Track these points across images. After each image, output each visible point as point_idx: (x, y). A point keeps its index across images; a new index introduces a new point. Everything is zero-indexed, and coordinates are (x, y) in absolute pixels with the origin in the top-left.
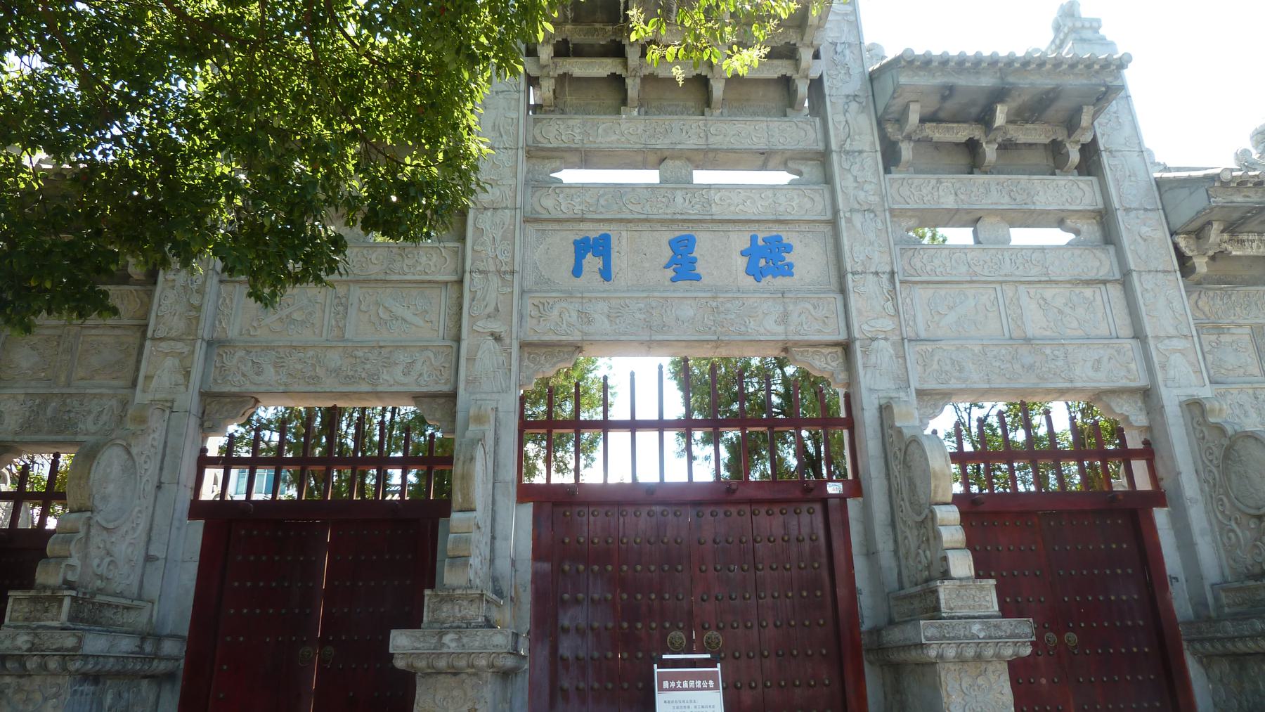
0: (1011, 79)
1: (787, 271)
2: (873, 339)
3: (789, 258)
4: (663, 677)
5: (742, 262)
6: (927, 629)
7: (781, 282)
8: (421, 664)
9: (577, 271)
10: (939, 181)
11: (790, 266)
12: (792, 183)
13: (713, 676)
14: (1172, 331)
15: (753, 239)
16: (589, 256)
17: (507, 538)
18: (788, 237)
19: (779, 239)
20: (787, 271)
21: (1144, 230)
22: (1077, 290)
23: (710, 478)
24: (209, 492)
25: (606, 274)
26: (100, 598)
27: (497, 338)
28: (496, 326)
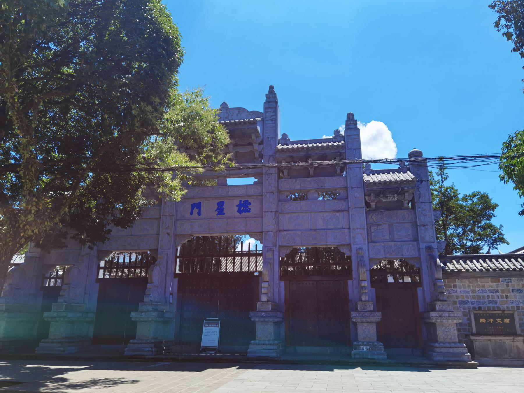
0: (310, 153)
1: (249, 211)
2: (268, 232)
3: (250, 207)
4: (206, 324)
5: (236, 208)
6: (433, 314)
7: (247, 214)
8: (137, 320)
9: (192, 213)
10: (296, 181)
11: (250, 209)
12: (255, 182)
13: (218, 324)
14: (359, 227)
15: (241, 201)
16: (195, 209)
17: (169, 288)
18: (250, 200)
19: (248, 201)
20: (249, 211)
21: (356, 194)
22: (334, 214)
23: (231, 270)
24: (101, 276)
25: (199, 214)
26: (72, 304)
27: (168, 234)
28: (168, 231)
